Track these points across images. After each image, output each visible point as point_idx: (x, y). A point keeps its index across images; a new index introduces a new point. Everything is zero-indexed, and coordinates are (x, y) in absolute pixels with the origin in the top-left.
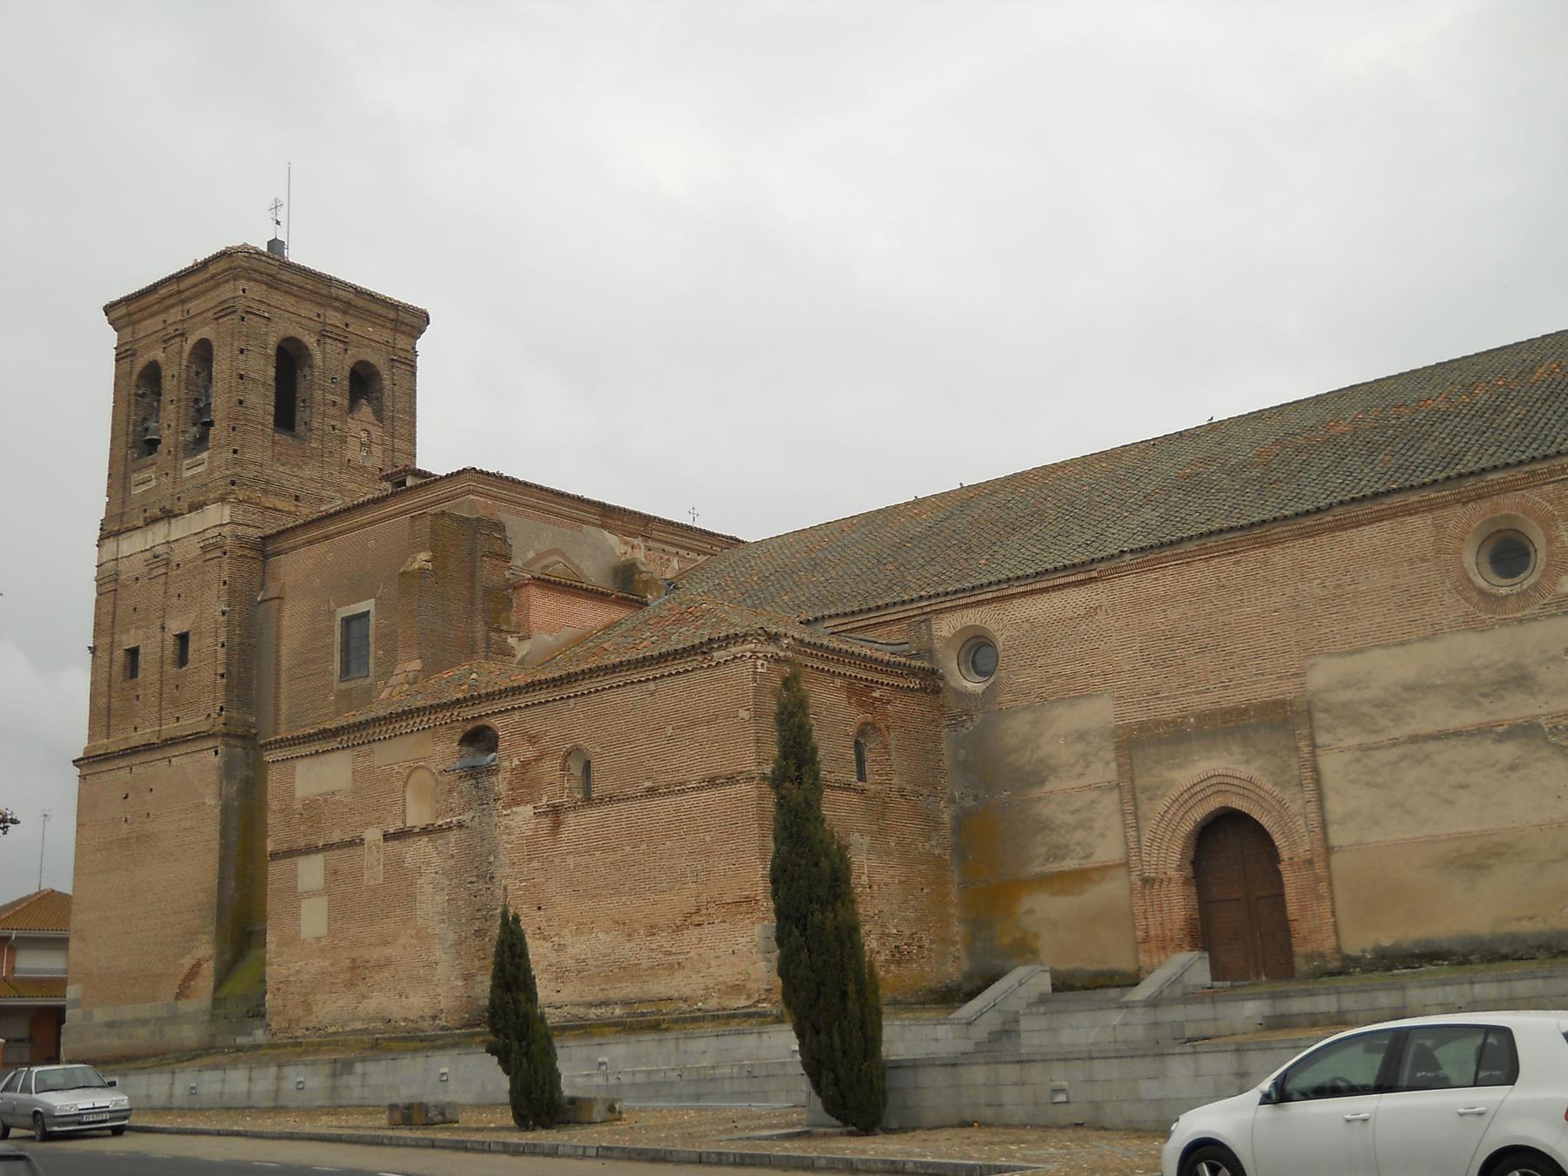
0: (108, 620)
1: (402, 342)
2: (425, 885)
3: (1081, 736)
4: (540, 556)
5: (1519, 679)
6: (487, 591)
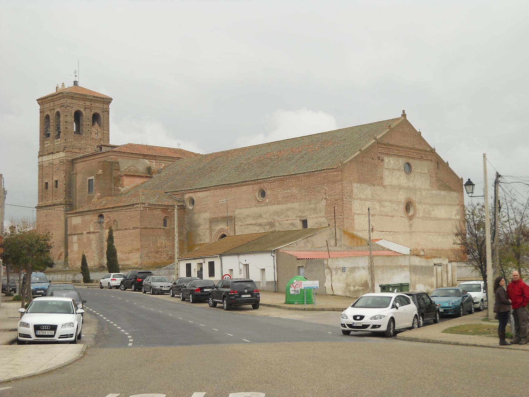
0: (41, 176)
1: (105, 106)
2: (93, 242)
3: (205, 219)
4: (128, 167)
5: (260, 216)
6: (114, 177)
